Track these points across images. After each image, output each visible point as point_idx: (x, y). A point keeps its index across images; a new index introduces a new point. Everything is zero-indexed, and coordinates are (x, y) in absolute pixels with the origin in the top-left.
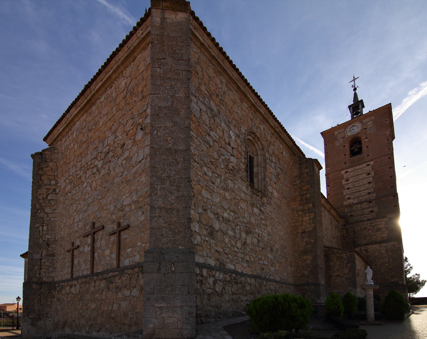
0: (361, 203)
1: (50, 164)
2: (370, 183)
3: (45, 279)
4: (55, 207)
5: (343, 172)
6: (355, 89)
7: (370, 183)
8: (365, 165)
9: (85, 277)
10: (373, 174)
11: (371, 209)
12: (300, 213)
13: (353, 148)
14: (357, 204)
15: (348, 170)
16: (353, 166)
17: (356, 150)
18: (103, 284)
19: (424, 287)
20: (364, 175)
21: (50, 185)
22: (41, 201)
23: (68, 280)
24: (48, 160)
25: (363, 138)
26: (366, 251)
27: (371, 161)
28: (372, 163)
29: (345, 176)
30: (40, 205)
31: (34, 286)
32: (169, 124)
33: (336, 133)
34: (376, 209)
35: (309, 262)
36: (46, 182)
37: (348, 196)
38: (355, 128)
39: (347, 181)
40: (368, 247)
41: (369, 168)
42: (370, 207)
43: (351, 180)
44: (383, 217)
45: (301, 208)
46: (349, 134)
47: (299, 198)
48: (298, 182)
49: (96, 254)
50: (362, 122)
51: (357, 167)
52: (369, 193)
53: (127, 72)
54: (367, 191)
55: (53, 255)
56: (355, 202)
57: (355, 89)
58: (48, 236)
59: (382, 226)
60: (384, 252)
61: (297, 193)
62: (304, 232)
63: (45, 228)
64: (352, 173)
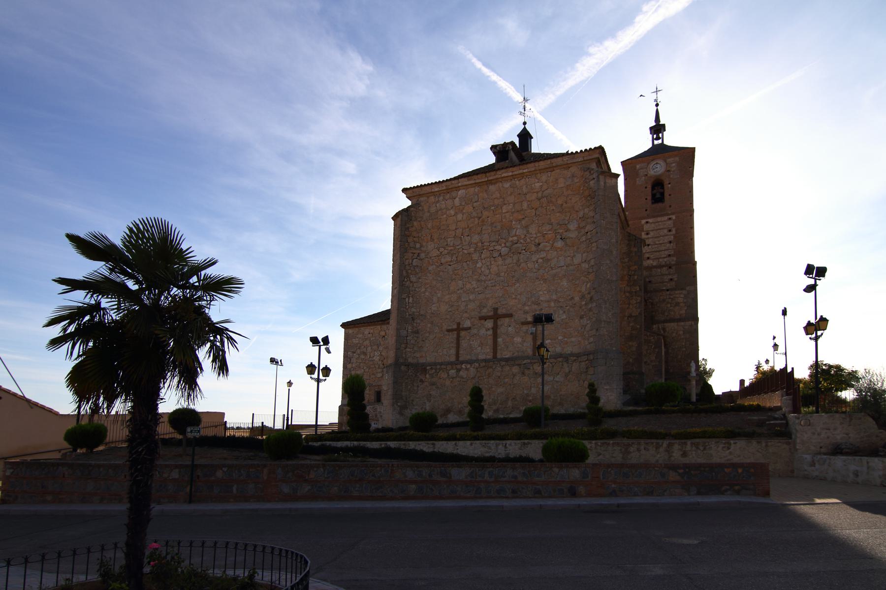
0: (661, 267)
1: (415, 223)
2: (670, 242)
3: (410, 360)
4: (420, 275)
5: (643, 221)
6: (657, 105)
7: (670, 242)
8: (666, 218)
9: (485, 361)
10: (674, 232)
11: (670, 277)
12: (628, 294)
13: (655, 191)
14: (655, 267)
15: (650, 220)
16: (654, 217)
17: (658, 196)
18: (515, 369)
19: (843, 366)
20: (666, 231)
21: (415, 248)
22: (408, 267)
23: (451, 363)
24: (413, 218)
25: (666, 182)
26: (664, 329)
27: (673, 214)
28: (674, 217)
29: (646, 227)
30: (407, 272)
31: (403, 368)
32: (608, 262)
33: (638, 167)
34: (675, 277)
35: (634, 349)
36: (412, 245)
37: (647, 255)
38: (658, 166)
39: (647, 234)
40: (667, 325)
41: (670, 222)
42: (670, 274)
43: (652, 234)
44: (682, 289)
45: (628, 289)
46: (652, 173)
47: (627, 278)
48: (626, 260)
49: (500, 340)
50: (665, 161)
51: (659, 219)
52: (669, 255)
53: (544, 178)
54: (667, 253)
55: (417, 332)
56: (655, 264)
57: (657, 105)
58: (413, 310)
59: (681, 300)
60: (681, 332)
61: (625, 273)
62: (630, 316)
63: (411, 299)
64: (653, 225)
